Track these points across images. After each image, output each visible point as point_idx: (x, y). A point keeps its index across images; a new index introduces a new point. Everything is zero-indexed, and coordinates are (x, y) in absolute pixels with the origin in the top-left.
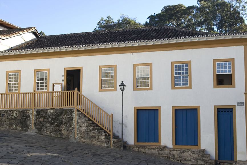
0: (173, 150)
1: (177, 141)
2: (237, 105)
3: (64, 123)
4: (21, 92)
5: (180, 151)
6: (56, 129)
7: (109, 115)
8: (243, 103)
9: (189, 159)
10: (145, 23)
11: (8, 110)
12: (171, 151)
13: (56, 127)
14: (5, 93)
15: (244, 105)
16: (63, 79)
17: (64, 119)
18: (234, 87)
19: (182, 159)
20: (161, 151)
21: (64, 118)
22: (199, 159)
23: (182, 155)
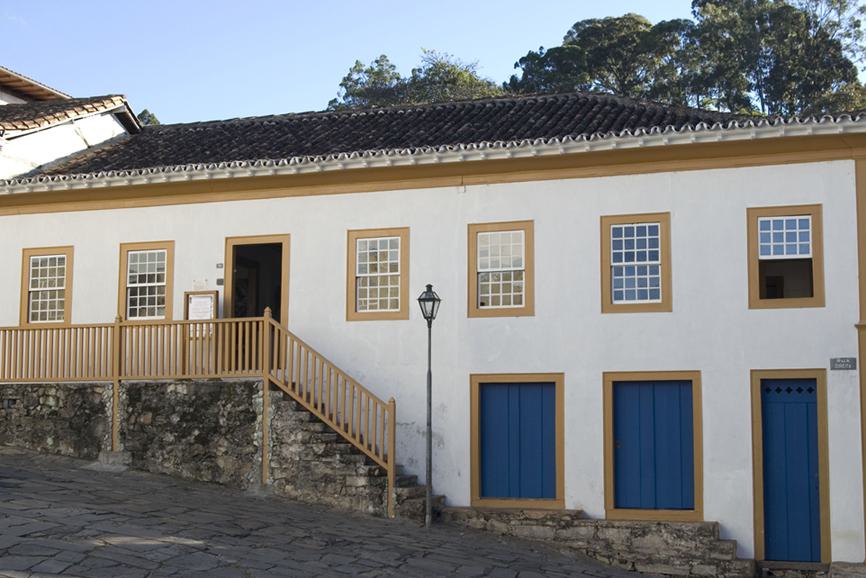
0: (607, 527)
1: (620, 494)
4: (75, 321)
5: (629, 530)
6: (196, 452)
8: (853, 361)
9: (663, 555)
11: (27, 385)
12: (598, 529)
14: (17, 324)
15: (854, 368)
16: (222, 277)
17: (223, 416)
19: (639, 557)
20: (564, 528)
21: (226, 414)
23: (637, 542)
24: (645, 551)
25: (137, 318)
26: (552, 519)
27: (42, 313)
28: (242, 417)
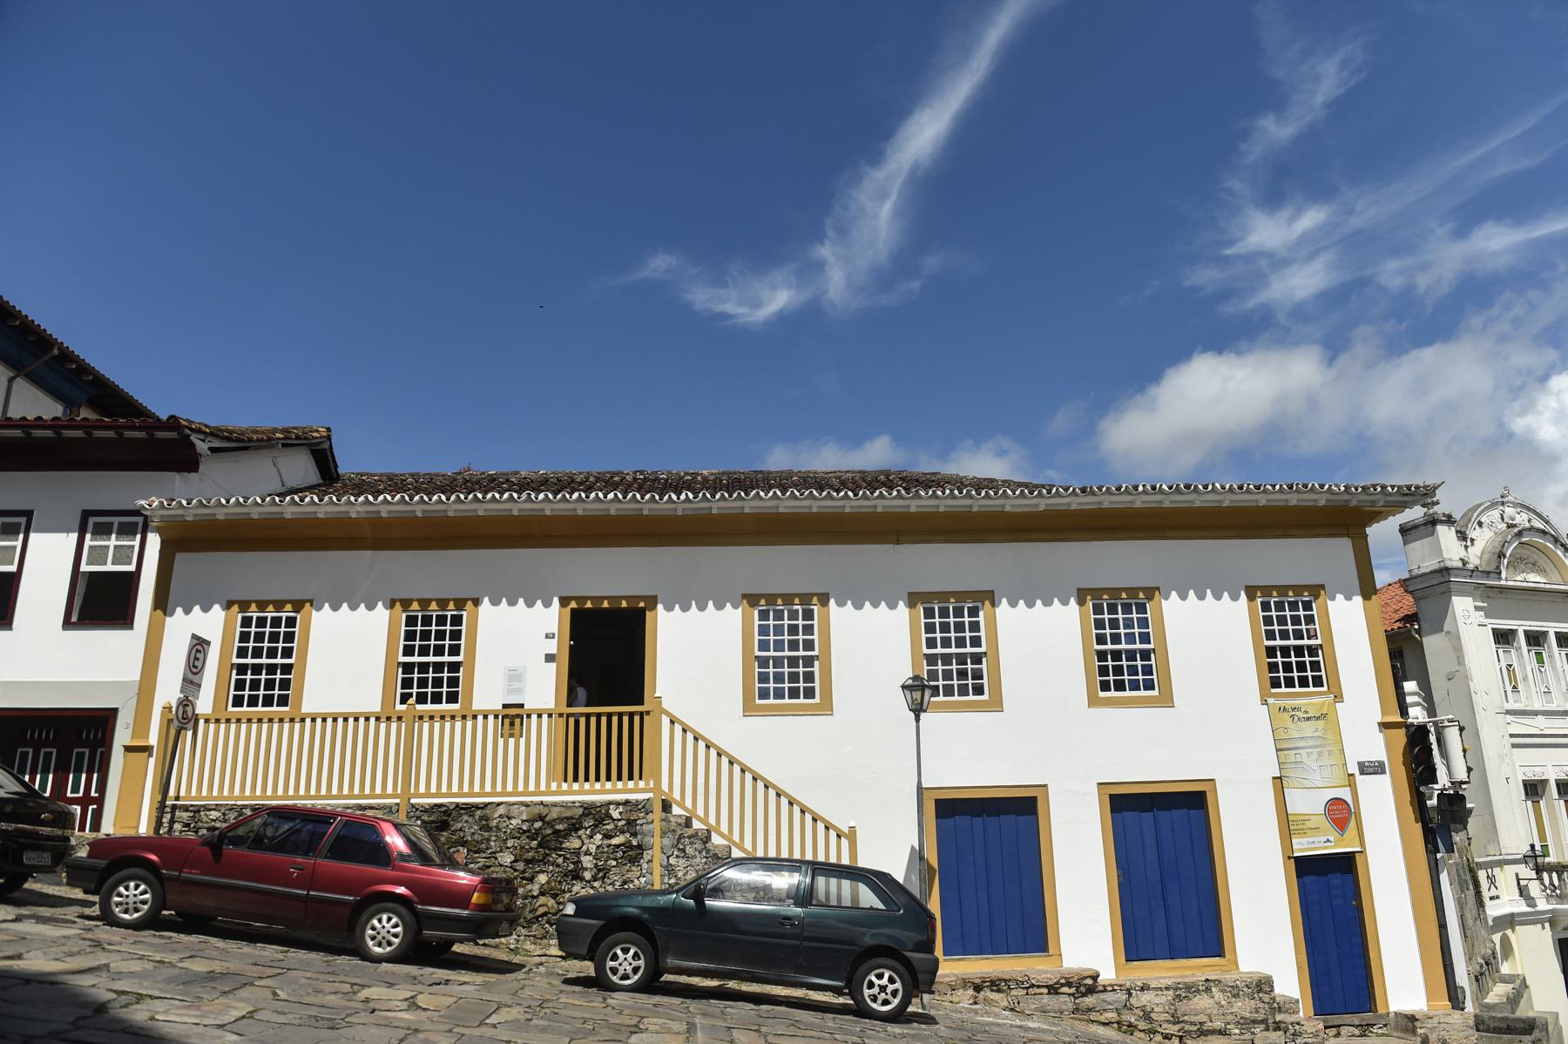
0: (1142, 989)
1: (1138, 941)
2: (1362, 773)
3: (587, 875)
4: (307, 707)
5: (1171, 993)
6: (541, 910)
7: (835, 828)
8: (1381, 764)
9: (1218, 1024)
10: (197, 608)
11: (245, 807)
12: (1130, 995)
13: (542, 900)
14: (551, 705)
15: (1383, 772)
16: (554, 651)
17: (587, 853)
18: (826, 707)
19: (1187, 1027)
20: (1084, 995)
21: (593, 849)
22: (1262, 1022)
23: (1183, 1007)
24: (1193, 1019)
25: (429, 707)
26: (1069, 984)
27: (1276, 664)
28: (620, 854)
